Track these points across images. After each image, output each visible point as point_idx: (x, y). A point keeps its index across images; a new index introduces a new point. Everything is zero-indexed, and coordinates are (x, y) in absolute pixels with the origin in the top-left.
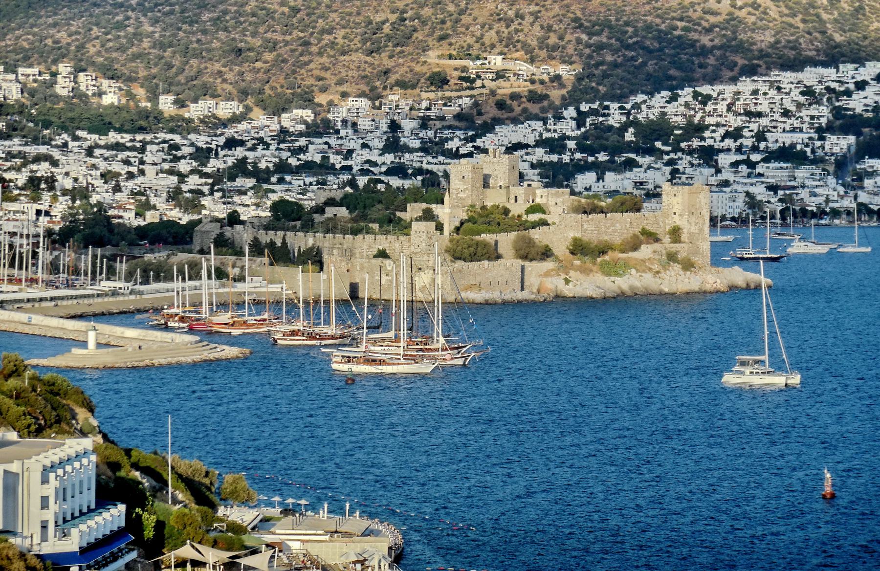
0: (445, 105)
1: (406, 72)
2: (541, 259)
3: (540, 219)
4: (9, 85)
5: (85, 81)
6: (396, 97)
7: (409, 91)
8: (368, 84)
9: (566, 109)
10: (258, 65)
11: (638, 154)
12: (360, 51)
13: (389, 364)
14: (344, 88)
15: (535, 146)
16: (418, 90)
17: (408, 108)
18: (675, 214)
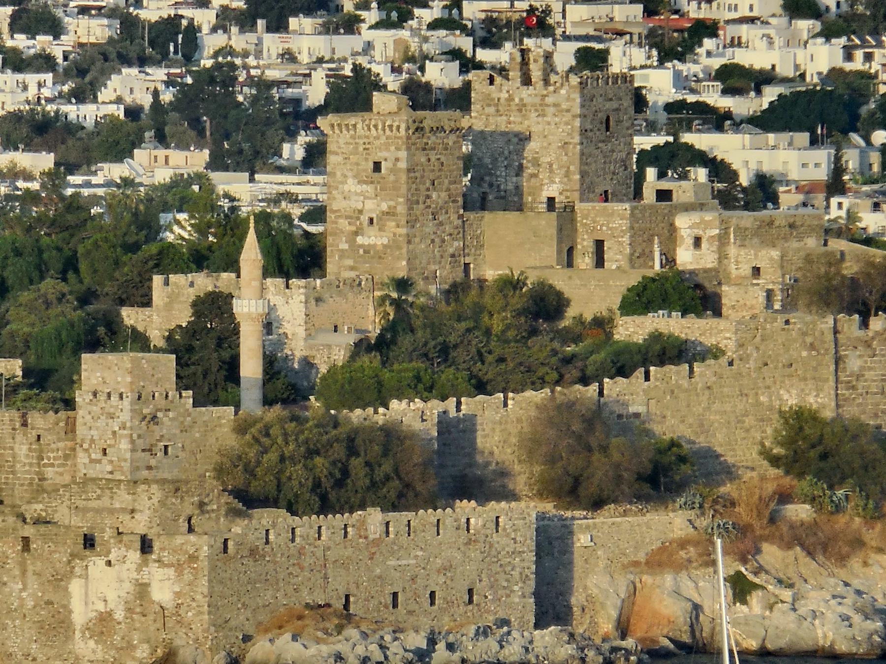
2: (640, 498)
3: (656, 337)
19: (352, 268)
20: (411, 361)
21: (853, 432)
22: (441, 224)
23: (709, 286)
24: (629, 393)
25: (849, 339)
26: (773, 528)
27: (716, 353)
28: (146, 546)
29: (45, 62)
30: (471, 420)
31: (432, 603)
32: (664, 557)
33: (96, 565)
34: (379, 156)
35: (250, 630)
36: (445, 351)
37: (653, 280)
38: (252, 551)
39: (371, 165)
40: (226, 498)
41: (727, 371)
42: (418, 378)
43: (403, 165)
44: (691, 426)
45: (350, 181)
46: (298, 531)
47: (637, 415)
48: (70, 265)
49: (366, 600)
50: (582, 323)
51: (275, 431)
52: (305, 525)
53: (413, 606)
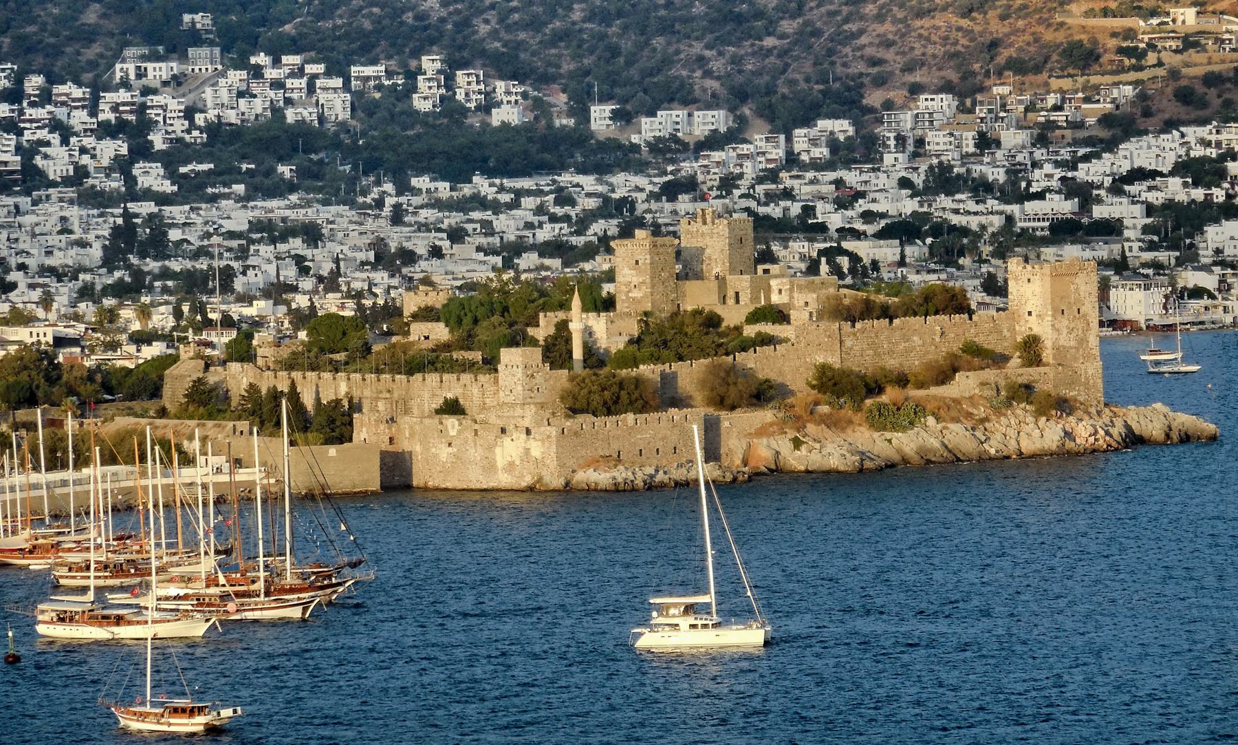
0: (1087, 100)
1: (1028, 44)
3: (759, 334)
4: (331, 96)
5: (467, 84)
6: (1005, 90)
7: (1030, 78)
8: (958, 68)
10: (769, 42)
12: (950, 9)
13: (130, 623)
14: (917, 77)
16: (1045, 75)
17: (1021, 108)
18: (1030, 313)
21: (845, 374)
24: (748, 360)
27: (786, 340)
28: (528, 432)
29: (567, 218)
30: (675, 374)
33: (507, 440)
34: (638, 258)
36: (665, 343)
38: (576, 433)
43: (648, 261)
48: (505, 309)
52: (599, 421)
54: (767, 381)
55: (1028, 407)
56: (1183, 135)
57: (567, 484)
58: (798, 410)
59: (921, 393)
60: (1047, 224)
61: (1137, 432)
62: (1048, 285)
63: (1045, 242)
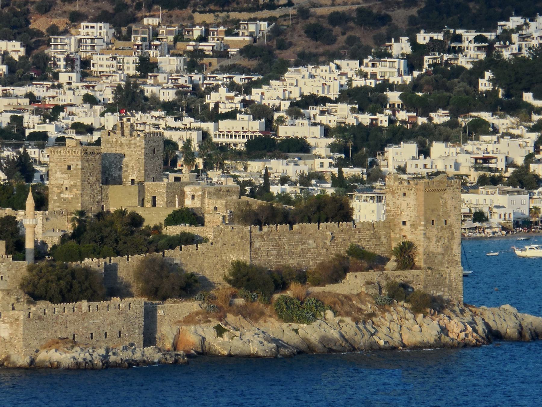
0: (229, 33)
2: (180, 296)
3: (184, 234)
7: (176, 12)
9: (397, 41)
11: (493, 110)
15: (336, 101)
16: (189, 10)
17: (171, 38)
18: (404, 223)
19: (59, 207)
20: (89, 243)
21: (259, 270)
22: (93, 190)
23: (199, 214)
24: (175, 255)
25: (255, 235)
26: (231, 308)
27: (207, 240)
31: (106, 337)
32: (190, 319)
34: (70, 163)
35: (39, 348)
36: (102, 239)
37: (177, 212)
38: (40, 318)
39: (67, 167)
40: (27, 297)
41: (210, 247)
42: (95, 250)
43: (79, 167)
44: (197, 268)
45: (58, 173)
46: (56, 309)
47: (177, 264)
49: (81, 336)
50: (150, 228)
51: (44, 271)
52: (58, 307)
53: (98, 338)
54: (192, 275)
55: (406, 305)
56: (338, 67)
57: (32, 361)
58: (219, 302)
59: (317, 290)
60: (245, 140)
61: (494, 329)
62: (422, 199)
63: (238, 155)
